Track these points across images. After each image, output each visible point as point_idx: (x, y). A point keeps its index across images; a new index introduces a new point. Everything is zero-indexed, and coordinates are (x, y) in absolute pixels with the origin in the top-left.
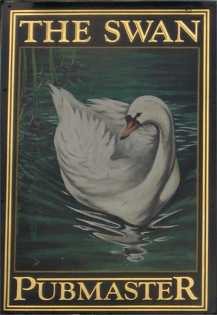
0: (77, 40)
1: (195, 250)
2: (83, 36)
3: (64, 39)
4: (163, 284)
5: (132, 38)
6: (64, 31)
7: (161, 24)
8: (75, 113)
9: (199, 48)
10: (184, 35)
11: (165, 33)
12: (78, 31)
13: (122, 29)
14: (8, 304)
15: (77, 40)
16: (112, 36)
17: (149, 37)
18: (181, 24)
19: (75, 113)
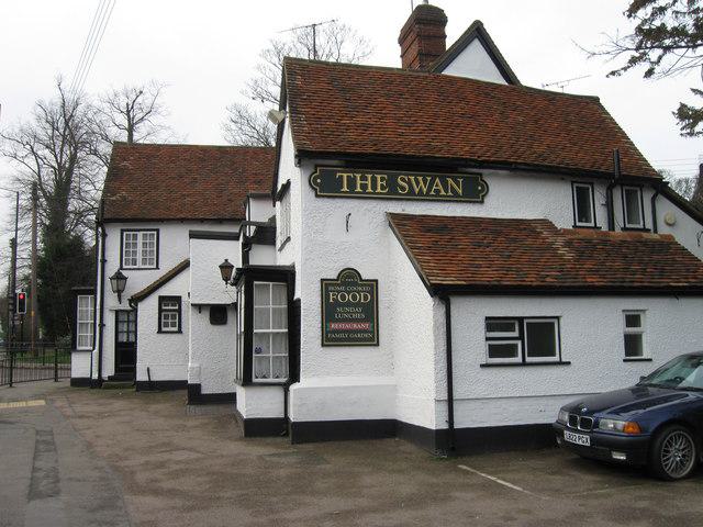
0: (379, 190)
1: (94, 292)
2: (382, 187)
3: (370, 190)
4: (330, 339)
5: (417, 190)
6: (369, 183)
7: (437, 180)
8: (289, 183)
9: (519, 359)
10: (453, 190)
11: (441, 187)
12: (379, 183)
13: (409, 183)
14: (638, 226)
15: (379, 190)
16: (403, 188)
17: (429, 190)
18: (450, 181)
19: (289, 183)
